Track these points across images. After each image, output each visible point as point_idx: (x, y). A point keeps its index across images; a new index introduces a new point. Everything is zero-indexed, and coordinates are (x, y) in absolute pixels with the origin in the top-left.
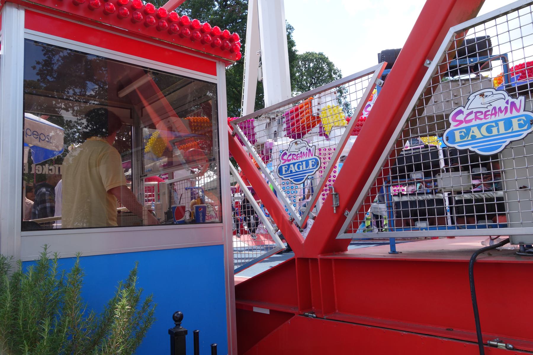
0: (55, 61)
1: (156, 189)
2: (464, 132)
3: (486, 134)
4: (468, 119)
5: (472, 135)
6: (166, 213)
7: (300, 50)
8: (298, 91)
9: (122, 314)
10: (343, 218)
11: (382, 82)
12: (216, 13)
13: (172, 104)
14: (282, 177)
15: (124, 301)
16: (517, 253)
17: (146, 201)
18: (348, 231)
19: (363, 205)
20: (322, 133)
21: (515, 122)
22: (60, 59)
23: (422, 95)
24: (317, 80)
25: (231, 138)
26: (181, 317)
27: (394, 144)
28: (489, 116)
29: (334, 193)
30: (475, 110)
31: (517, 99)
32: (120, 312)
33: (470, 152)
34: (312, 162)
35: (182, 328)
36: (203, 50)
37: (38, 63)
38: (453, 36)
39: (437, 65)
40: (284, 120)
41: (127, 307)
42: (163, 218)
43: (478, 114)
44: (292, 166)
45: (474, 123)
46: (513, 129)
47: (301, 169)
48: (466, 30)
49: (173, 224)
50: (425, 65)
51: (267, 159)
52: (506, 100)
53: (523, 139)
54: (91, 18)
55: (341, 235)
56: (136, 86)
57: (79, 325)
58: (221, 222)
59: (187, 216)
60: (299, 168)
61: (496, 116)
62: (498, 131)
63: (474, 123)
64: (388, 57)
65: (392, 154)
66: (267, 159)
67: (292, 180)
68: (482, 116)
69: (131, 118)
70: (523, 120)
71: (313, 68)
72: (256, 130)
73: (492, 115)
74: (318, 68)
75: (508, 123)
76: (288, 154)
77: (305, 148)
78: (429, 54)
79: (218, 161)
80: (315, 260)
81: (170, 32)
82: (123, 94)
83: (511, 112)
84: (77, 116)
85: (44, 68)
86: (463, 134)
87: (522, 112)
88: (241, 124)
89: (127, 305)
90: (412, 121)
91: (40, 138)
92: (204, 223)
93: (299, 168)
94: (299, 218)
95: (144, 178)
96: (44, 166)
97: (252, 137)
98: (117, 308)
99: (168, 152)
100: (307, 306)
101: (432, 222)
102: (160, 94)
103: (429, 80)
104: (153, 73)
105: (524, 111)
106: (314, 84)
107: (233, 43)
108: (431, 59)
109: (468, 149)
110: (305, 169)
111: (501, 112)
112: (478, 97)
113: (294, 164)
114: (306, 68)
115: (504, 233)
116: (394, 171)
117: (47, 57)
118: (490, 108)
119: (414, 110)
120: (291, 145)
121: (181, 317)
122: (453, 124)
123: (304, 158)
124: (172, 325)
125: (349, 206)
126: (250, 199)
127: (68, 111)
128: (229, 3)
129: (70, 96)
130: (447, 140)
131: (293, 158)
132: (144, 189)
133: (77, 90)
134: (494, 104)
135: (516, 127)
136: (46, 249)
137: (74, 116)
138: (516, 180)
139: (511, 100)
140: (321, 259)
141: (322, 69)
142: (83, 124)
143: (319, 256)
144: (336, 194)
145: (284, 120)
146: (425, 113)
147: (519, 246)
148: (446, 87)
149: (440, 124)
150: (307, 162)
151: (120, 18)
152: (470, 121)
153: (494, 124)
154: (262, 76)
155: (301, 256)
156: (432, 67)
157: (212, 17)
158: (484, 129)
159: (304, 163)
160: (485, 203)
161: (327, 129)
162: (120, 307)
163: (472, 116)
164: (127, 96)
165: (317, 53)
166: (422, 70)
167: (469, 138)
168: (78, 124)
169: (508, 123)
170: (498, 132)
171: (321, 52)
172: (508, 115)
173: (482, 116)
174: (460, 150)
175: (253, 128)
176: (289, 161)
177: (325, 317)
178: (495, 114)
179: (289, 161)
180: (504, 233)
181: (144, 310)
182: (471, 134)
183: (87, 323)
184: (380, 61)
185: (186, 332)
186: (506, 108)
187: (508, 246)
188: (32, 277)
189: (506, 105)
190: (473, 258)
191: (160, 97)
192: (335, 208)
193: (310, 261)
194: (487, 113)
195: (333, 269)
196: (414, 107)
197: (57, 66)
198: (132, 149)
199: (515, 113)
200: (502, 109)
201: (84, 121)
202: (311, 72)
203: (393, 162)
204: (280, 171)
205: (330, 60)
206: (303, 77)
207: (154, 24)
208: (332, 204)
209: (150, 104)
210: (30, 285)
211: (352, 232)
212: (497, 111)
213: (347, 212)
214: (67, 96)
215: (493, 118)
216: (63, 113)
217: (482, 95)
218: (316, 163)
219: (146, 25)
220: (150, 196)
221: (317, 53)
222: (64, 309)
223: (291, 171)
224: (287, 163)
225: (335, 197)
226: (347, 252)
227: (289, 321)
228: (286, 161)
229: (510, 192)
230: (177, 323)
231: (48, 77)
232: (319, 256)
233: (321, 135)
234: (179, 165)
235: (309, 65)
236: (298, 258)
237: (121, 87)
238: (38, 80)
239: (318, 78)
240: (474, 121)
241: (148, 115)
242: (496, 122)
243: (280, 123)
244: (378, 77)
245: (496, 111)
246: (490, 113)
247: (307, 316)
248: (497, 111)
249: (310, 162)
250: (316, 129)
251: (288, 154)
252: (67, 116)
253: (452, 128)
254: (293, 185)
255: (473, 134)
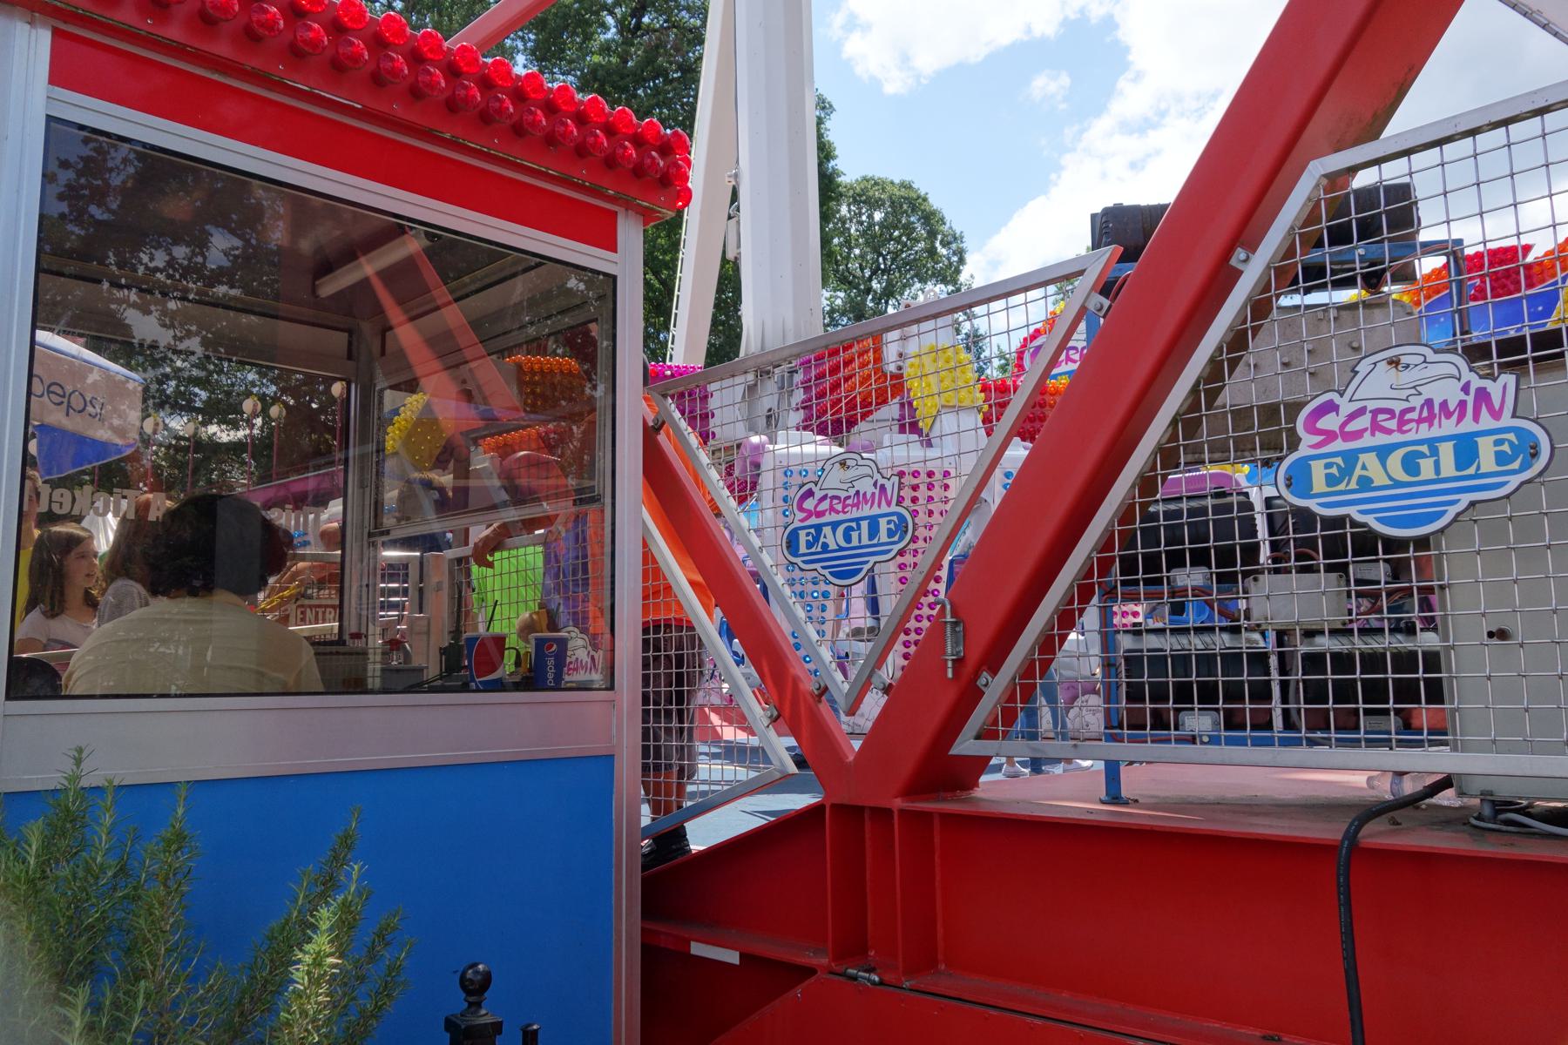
0: (118, 161)
1: (413, 572)
2: (1338, 466)
3: (1402, 476)
4: (1350, 428)
5: (1360, 477)
6: (443, 651)
7: (850, 169)
8: (835, 290)
9: (315, 982)
10: (970, 696)
11: (1106, 303)
12: (606, 49)
13: (476, 325)
14: (798, 560)
15: (321, 942)
16: (1474, 822)
17: (382, 609)
18: (986, 734)
19: (1033, 661)
20: (910, 425)
21: (1486, 448)
22: (132, 156)
23: (1219, 349)
24: (893, 260)
25: (650, 434)
26: (487, 980)
27: (1133, 486)
28: (1413, 425)
29: (949, 618)
30: (1372, 405)
31: (1495, 380)
32: (308, 973)
33: (1354, 524)
34: (889, 522)
35: (485, 1016)
36: (582, 174)
37: (64, 164)
38: (1317, 185)
39: (1268, 267)
40: (799, 377)
41: (331, 960)
42: (433, 671)
43: (1381, 417)
44: (827, 530)
45: (1368, 440)
46: (1478, 468)
47: (855, 543)
48: (1353, 170)
49: (465, 688)
50: (1233, 262)
51: (744, 490)
52: (1463, 381)
53: (1507, 497)
54: (252, 63)
55: (965, 745)
56: (368, 268)
57: (176, 1003)
58: (611, 688)
59: (508, 666)
60: (848, 539)
61: (1431, 425)
62: (1437, 470)
63: (1368, 440)
64: (1122, 230)
65: (1126, 515)
66: (744, 490)
67: (826, 572)
68: (1392, 424)
69: (350, 357)
70: (1511, 443)
71: (881, 224)
72: (713, 403)
73: (1419, 421)
74: (896, 228)
75: (1466, 450)
76: (818, 494)
77: (871, 482)
78: (1247, 234)
79: (608, 500)
80: (883, 814)
81: (485, 118)
82: (330, 286)
83: (1476, 418)
84: (172, 326)
85: (83, 181)
86: (1334, 470)
87: (1506, 420)
88: (682, 395)
89: (331, 955)
90: (1187, 422)
91: (69, 406)
92: (557, 688)
93: (848, 539)
94: (841, 685)
95: (381, 539)
96: (77, 493)
97: (701, 420)
98: (299, 961)
99: (451, 455)
100: (852, 948)
101: (1233, 722)
102: (441, 293)
103: (1244, 307)
104: (427, 233)
105: (1514, 416)
106: (884, 272)
107: (670, 159)
108: (1252, 247)
109: (1348, 516)
110: (865, 541)
111: (1449, 415)
112: (1383, 366)
113: (834, 526)
114: (861, 223)
115: (1432, 761)
116: (1129, 566)
117: (95, 150)
118: (1417, 402)
119: (1195, 390)
120: (827, 467)
121: (487, 980)
122: (1307, 440)
123: (866, 511)
124: (457, 1002)
125: (993, 660)
126: (697, 617)
127: (147, 312)
128: (646, 20)
129: (157, 269)
130: (1288, 486)
131: (832, 509)
132: (379, 572)
133: (181, 252)
134: (1427, 392)
135: (1487, 461)
136: (78, 762)
137: (164, 326)
138: (1483, 615)
139: (1477, 382)
140: (902, 812)
141: (908, 229)
142: (193, 353)
143: (898, 803)
144: (955, 624)
145: (799, 377)
146: (1226, 398)
147: (1477, 801)
148: (1289, 328)
149: (1269, 433)
150: (874, 522)
151: (338, 68)
152: (1358, 434)
153: (1424, 449)
154: (739, 246)
155: (844, 798)
156: (1253, 269)
157: (597, 59)
158: (1395, 460)
159: (864, 525)
160: (1390, 675)
161: (924, 408)
162: (308, 959)
163: (1364, 422)
164: (341, 294)
165: (897, 181)
166: (1222, 279)
167: (1353, 485)
168: (177, 352)
169: (1466, 450)
170: (1437, 471)
171: (907, 178)
172: (1468, 426)
173: (1392, 424)
174: (1324, 520)
175: (705, 398)
176: (820, 514)
177: (907, 984)
178: (1430, 420)
179: (820, 514)
180: (1432, 761)
181: (373, 956)
182: (1358, 472)
183: (202, 1000)
184: (1096, 244)
185: (497, 1028)
186: (1462, 405)
187: (1447, 798)
188: (38, 856)
189: (1462, 396)
190: (1352, 835)
191: (439, 302)
192: (950, 664)
193: (867, 815)
194: (1408, 416)
195: (937, 840)
196: (1197, 383)
197: (122, 177)
198: (345, 445)
199: (1486, 421)
200: (1452, 408)
201: (194, 344)
202: (885, 243)
203: (1128, 540)
204: (792, 544)
205: (935, 202)
206: (850, 249)
207: (442, 91)
208: (944, 653)
209: (412, 319)
210: (31, 882)
211: (997, 738)
212: (1437, 410)
213: (985, 677)
214: (147, 268)
215: (1424, 432)
216: (132, 316)
217: (1394, 362)
218: (901, 527)
219: (415, 93)
220: (394, 592)
221: (897, 181)
222: (128, 951)
223: (825, 546)
224: (814, 521)
225: (953, 631)
226: (978, 793)
227: (798, 992)
228: (810, 514)
229: (1459, 636)
230: (471, 999)
231: (93, 209)
232: (898, 803)
233: (902, 430)
234: (488, 509)
235: (870, 217)
236: (833, 806)
237: (326, 266)
238: (62, 216)
239: (896, 255)
240: (1367, 434)
241: (401, 354)
242: (1433, 443)
243: (785, 389)
244: (1093, 288)
245: (1431, 412)
246: (1415, 415)
247: (855, 978)
248: (1437, 410)
249: (883, 522)
250: (891, 410)
251: (818, 494)
252: (145, 326)
253: (1303, 450)
254: (830, 588)
255: (1364, 473)
